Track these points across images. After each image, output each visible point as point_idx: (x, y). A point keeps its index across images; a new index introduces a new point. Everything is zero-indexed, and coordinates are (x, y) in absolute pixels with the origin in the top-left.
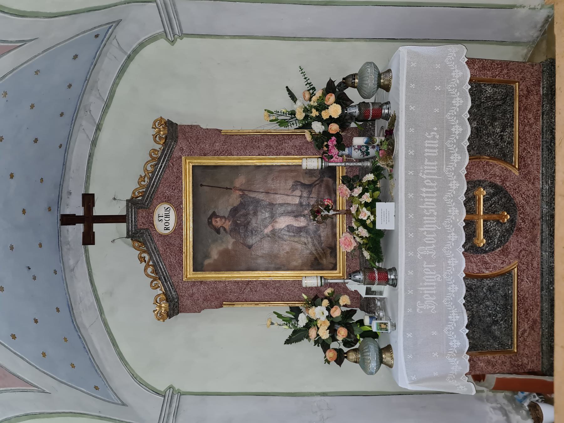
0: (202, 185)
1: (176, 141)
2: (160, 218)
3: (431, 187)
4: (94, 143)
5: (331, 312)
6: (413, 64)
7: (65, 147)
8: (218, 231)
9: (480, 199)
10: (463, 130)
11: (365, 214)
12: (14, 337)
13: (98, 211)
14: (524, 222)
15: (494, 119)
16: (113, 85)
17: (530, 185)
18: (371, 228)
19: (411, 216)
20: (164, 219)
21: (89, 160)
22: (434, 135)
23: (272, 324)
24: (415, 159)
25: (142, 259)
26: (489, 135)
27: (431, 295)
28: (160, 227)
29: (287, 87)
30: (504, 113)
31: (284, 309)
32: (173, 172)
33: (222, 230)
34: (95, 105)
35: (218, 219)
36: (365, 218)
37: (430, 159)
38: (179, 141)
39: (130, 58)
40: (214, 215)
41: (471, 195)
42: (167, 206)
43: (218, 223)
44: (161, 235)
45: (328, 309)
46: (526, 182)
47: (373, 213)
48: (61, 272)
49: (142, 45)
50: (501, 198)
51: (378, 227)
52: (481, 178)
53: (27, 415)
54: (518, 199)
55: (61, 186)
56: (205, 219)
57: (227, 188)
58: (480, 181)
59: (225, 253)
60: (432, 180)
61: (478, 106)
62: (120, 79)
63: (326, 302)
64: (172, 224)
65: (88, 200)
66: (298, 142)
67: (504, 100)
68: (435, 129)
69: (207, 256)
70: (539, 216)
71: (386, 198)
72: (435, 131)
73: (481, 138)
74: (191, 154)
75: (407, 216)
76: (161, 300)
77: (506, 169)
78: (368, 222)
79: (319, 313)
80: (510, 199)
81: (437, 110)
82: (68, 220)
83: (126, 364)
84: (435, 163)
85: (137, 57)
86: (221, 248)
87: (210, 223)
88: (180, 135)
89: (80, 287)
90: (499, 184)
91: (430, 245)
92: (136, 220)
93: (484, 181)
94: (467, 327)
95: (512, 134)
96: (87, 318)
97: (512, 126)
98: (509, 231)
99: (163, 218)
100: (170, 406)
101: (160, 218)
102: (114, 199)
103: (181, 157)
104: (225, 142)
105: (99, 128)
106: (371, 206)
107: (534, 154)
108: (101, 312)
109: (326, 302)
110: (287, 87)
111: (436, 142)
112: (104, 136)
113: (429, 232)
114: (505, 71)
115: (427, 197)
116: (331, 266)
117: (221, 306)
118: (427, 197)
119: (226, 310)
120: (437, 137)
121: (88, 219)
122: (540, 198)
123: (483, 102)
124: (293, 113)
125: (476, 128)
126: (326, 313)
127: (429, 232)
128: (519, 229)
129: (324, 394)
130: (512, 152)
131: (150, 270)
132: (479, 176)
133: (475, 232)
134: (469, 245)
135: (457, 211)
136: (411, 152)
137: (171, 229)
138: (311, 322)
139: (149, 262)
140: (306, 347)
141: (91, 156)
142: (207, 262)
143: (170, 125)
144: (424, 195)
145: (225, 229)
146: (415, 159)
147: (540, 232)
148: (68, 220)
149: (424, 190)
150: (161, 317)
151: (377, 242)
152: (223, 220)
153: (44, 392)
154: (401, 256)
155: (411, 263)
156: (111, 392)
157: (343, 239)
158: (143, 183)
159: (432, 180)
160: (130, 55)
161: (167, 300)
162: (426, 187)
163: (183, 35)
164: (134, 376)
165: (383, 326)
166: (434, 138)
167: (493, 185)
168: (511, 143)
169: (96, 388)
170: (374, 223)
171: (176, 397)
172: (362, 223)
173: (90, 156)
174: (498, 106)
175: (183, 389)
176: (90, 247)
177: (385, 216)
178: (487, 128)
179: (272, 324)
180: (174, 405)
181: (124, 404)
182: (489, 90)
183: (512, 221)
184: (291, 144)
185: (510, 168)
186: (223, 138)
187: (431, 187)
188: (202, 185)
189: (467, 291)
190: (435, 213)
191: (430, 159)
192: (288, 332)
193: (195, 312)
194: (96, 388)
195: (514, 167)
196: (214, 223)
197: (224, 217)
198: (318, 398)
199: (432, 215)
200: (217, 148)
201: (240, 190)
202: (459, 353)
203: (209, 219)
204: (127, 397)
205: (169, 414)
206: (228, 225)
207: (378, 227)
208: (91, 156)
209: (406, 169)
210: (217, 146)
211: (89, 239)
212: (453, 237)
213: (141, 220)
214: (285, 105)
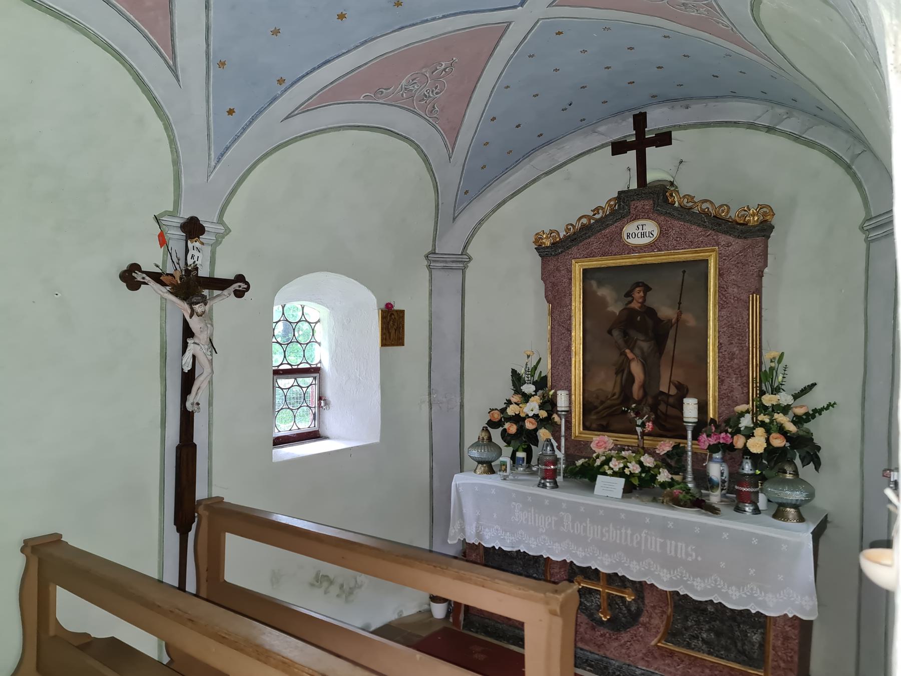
0: (684, 272)
1: (739, 237)
2: (640, 227)
3: (632, 541)
4: (751, 126)
5: (531, 419)
6: (784, 547)
7: (734, 95)
8: (629, 294)
9: (622, 592)
10: (699, 590)
11: (616, 465)
12: (494, 119)
13: (651, 151)
14: (601, 636)
15: (718, 634)
16: (821, 145)
17: (640, 655)
18: (600, 471)
19: (601, 512)
20: (641, 232)
21: (730, 122)
22: (691, 556)
23: (528, 356)
24: (663, 529)
25: (596, 210)
26: (698, 623)
27: (527, 520)
28: (630, 228)
29: (814, 385)
30: (727, 649)
31: (546, 368)
32: (699, 236)
33: (630, 299)
34: (791, 125)
35: (642, 294)
36: (611, 465)
37: (663, 546)
38: (740, 241)
39: (848, 168)
40: (647, 289)
41: (628, 584)
42: (656, 234)
43: (638, 294)
44: (620, 233)
45: (536, 416)
46: (644, 651)
47: (615, 474)
48: (585, 125)
49: (859, 186)
50: (625, 617)
51: (600, 477)
52: (646, 601)
53: (426, 156)
54: (625, 636)
55: (691, 98)
56: (641, 278)
57: (680, 303)
58: (643, 598)
59: (603, 302)
60: (639, 543)
61: (734, 620)
62: (827, 155)
63: (543, 414)
64: (633, 241)
65: (664, 139)
66: (737, 394)
67: (743, 652)
68: (699, 559)
69: (600, 284)
70: (608, 654)
71: (629, 490)
72: (696, 558)
73: (695, 612)
74: (721, 258)
75: (601, 508)
76: (554, 237)
77: (658, 632)
78: (606, 467)
79: (533, 407)
80: (626, 627)
81: (723, 565)
82: (640, 121)
83: (494, 211)
84: (658, 550)
85: (848, 178)
86: (609, 299)
87: (637, 284)
88: (749, 241)
89: (577, 144)
90: (641, 619)
91: (573, 528)
92: (649, 197)
93: (643, 602)
94: (500, 548)
95: (699, 650)
96: (541, 161)
97: (710, 653)
98: (591, 616)
99: (640, 230)
100: (453, 262)
101: (640, 227)
102: (681, 162)
103: (718, 245)
104: (739, 300)
105: (770, 129)
106: (620, 474)
107: (677, 670)
108: (547, 173)
109: (543, 414)
110: (814, 385)
111: (684, 556)
112: (762, 139)
113: (585, 528)
114: (782, 665)
115: (621, 534)
116: (588, 424)
117: (548, 302)
118: (621, 534)
119: (546, 307)
120: (690, 559)
121: (641, 140)
122: (628, 662)
123: (739, 627)
124: (776, 390)
125: (705, 610)
126: (531, 414)
127: (585, 528)
128: (593, 628)
129: (462, 406)
130: (677, 644)
131: (584, 221)
132: (649, 600)
133: (589, 579)
134: (577, 570)
135: (607, 563)
136: (670, 525)
137: (629, 240)
138: (526, 398)
139: (594, 219)
140: (508, 391)
141: (736, 124)
142: (594, 284)
143: (765, 229)
144: (623, 531)
145: (630, 302)
146: (663, 529)
147: (592, 650)
148: (640, 121)
149: (629, 532)
150: (538, 240)
151: (585, 474)
152: (640, 301)
153: (450, 158)
154: (568, 496)
155: (555, 506)
156: (465, 204)
157: (606, 438)
158: (686, 200)
159: (639, 543)
160: (851, 168)
161: (553, 244)
162: (632, 535)
163: (868, 242)
164: (481, 223)
165: (503, 467)
166: (687, 554)
167: (639, 613)
168: (688, 646)
169: (466, 192)
170: (605, 474)
171: (461, 265)
172: (607, 462)
173: (735, 123)
174: (736, 643)
175: (468, 271)
176: (609, 149)
177: (609, 486)
178: (708, 622)
179: (528, 356)
180: (454, 265)
181: (454, 219)
182: (756, 638)
183: (601, 623)
184: (735, 385)
185: (659, 636)
186: (744, 297)
187: (632, 541)
188: (684, 272)
189: (534, 556)
190: (604, 539)
191: (663, 546)
192: (521, 371)
193: (542, 274)
194: (466, 192)
195: (659, 641)
196: (638, 289)
197: (644, 300)
198: (458, 400)
199: (603, 535)
200: (730, 290)
201: (678, 320)
202: (479, 535)
203: (643, 283)
204: (460, 221)
205: (446, 262)
206: (635, 305)
207: (600, 477)
208: (736, 124)
209: (652, 516)
210: (733, 290)
211: (619, 148)
212: (580, 553)
213: (639, 204)
214: (797, 378)
